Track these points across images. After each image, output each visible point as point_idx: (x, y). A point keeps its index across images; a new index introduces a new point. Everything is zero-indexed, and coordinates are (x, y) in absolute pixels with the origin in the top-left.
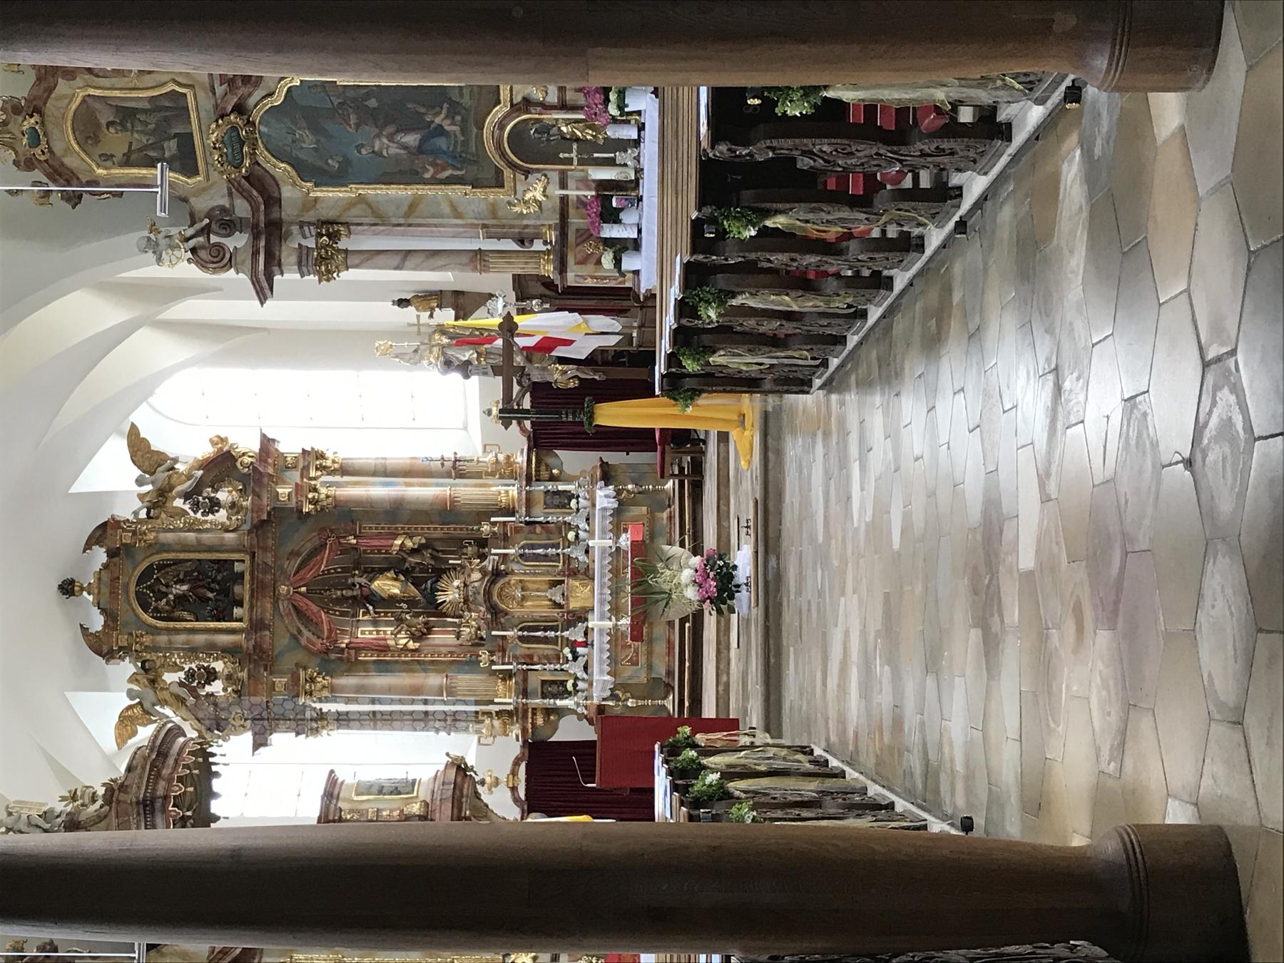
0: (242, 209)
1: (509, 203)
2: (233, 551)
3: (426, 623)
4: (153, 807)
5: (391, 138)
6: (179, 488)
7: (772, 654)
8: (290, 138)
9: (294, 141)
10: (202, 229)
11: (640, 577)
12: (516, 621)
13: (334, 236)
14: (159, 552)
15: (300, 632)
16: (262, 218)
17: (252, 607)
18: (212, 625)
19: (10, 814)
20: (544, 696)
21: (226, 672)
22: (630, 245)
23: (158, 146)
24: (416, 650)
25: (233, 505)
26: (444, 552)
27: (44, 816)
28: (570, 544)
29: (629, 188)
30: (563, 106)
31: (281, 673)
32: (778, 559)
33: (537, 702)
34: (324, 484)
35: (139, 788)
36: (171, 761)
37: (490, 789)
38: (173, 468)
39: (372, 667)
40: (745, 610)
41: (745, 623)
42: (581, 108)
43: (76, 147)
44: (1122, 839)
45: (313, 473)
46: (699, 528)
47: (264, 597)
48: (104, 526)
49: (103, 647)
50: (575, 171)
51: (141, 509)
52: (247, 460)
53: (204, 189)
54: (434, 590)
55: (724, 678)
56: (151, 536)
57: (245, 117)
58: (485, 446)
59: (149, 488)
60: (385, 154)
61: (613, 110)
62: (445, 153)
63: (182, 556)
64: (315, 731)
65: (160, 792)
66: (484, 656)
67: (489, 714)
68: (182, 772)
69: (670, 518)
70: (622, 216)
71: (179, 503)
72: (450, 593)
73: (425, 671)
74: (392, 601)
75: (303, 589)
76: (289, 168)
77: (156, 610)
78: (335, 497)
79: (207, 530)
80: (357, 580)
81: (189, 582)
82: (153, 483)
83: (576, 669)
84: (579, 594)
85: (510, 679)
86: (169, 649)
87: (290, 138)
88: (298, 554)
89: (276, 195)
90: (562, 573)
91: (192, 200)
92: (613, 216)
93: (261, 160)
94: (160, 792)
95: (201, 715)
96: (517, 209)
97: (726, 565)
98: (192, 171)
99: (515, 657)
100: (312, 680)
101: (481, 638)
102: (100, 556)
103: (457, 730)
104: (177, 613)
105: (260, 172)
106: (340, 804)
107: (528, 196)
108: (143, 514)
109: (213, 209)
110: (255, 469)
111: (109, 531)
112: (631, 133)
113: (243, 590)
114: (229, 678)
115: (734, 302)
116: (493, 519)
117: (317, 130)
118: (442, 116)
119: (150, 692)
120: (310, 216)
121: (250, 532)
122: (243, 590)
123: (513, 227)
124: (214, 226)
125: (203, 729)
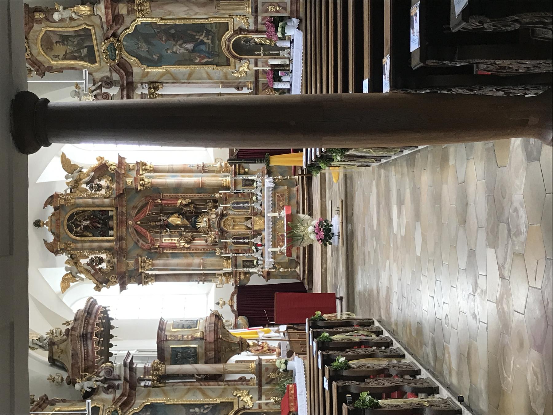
0: (116, 77)
1: (233, 73)
2: (108, 207)
3: (192, 236)
5: (181, 45)
7: (350, 266)
8: (136, 47)
9: (138, 48)
12: (231, 235)
13: (156, 88)
15: (138, 241)
16: (125, 82)
17: (117, 230)
18: (100, 238)
20: (244, 267)
21: (107, 259)
22: (286, 91)
23: (79, 51)
24: (188, 248)
25: (108, 187)
26: (199, 205)
27: (40, 339)
29: (286, 69)
30: (256, 31)
34: (147, 177)
35: (80, 329)
36: (93, 316)
38: (81, 171)
41: (336, 250)
42: (265, 32)
43: (42, 52)
45: (141, 172)
48: (52, 197)
50: (262, 59)
51: (68, 189)
52: (113, 167)
53: (99, 69)
54: (195, 222)
55: (325, 266)
56: (73, 201)
57: (117, 39)
59: (71, 179)
60: (178, 52)
61: (279, 35)
62: (204, 52)
63: (86, 209)
64: (146, 283)
65: (89, 330)
66: (218, 251)
67: (220, 275)
68: (98, 321)
69: (298, 190)
70: (282, 78)
71: (84, 186)
72: (202, 223)
73: (193, 256)
74: (177, 226)
75: (139, 222)
76: (136, 59)
77: (76, 232)
78: (151, 183)
79: (97, 198)
80: (162, 218)
82: (72, 178)
83: (257, 255)
84: (258, 224)
85: (229, 260)
86: (82, 249)
87: (136, 47)
91: (94, 74)
92: (278, 79)
93: (123, 56)
94: (89, 330)
95: (97, 277)
96: (236, 75)
98: (93, 61)
99: (231, 250)
100: (145, 262)
101: (216, 242)
102: (51, 209)
103: (207, 281)
104: (85, 233)
105: (124, 61)
106: (166, 333)
108: (69, 191)
109: (102, 78)
110: (116, 171)
111: (55, 199)
112: (287, 44)
113: (113, 223)
114: (109, 262)
115: (348, 153)
116: (220, 192)
117: (148, 42)
118: (203, 36)
119: (75, 268)
120: (146, 80)
121: (115, 198)
122: (113, 223)
125: (98, 283)
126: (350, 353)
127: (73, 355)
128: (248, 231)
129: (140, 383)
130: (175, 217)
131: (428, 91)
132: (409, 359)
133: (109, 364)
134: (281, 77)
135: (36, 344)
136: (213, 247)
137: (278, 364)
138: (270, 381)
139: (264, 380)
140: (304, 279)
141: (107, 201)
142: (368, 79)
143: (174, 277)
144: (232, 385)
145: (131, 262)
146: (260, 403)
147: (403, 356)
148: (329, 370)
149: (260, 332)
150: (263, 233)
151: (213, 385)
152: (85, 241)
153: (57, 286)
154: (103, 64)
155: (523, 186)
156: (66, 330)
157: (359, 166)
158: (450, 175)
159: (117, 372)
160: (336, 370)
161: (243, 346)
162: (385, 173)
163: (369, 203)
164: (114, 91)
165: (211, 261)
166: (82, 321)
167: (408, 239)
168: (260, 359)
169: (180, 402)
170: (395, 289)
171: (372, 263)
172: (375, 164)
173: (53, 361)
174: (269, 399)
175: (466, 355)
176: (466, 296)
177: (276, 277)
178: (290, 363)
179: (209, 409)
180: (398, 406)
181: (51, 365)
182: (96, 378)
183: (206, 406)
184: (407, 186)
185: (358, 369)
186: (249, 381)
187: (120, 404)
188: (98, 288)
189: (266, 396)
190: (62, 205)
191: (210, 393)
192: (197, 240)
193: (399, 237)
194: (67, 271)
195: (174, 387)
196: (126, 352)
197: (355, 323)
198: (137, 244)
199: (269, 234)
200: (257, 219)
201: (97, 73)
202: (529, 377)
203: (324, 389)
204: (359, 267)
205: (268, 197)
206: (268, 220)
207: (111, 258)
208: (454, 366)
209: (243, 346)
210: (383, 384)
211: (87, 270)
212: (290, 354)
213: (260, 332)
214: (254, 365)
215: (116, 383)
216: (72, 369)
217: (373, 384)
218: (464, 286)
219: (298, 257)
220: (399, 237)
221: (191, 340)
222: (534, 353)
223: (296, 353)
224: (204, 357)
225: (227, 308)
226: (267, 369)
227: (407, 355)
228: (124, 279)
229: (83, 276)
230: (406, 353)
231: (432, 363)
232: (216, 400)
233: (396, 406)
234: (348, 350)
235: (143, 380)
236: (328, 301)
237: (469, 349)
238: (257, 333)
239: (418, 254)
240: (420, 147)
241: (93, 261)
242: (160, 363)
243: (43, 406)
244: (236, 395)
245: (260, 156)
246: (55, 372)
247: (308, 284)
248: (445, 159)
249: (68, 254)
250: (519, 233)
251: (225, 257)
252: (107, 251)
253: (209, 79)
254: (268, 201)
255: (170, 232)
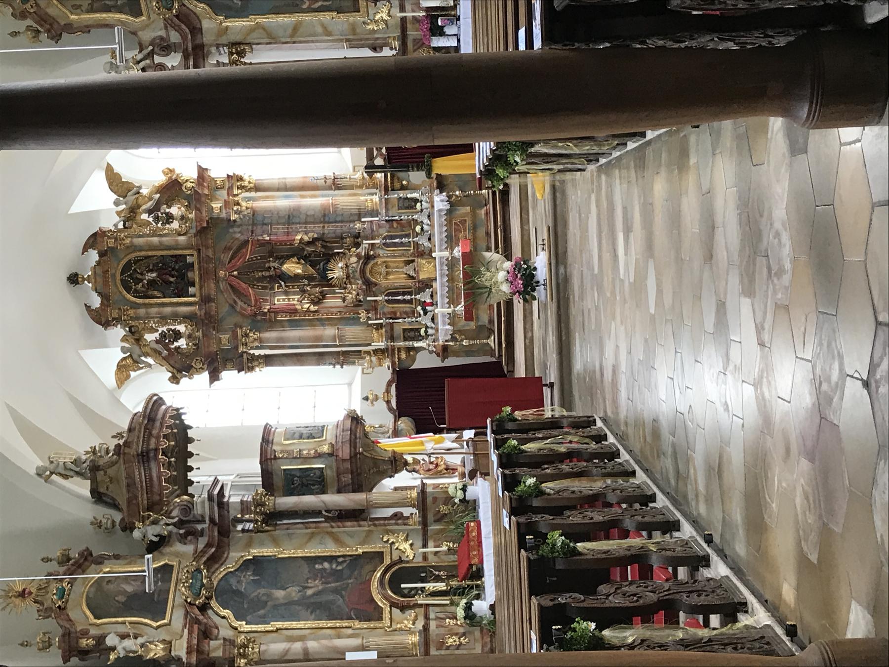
0: (175, 37)
1: (364, 23)
2: (185, 249)
3: (321, 292)
4: (148, 457)
6: (144, 207)
7: (563, 333)
10: (148, 54)
11: (469, 277)
13: (241, 54)
14: (134, 251)
15: (235, 302)
16: (190, 45)
17: (201, 288)
19: (52, 462)
20: (405, 339)
21: (187, 332)
25: (183, 218)
27: (76, 462)
28: (417, 235)
31: (225, 332)
32: (565, 267)
33: (401, 344)
35: (138, 444)
36: (158, 424)
37: (372, 403)
38: (139, 193)
39: (287, 324)
40: (543, 298)
41: (543, 307)
44: (822, 654)
45: (235, 192)
46: (507, 217)
47: (209, 279)
48: (95, 235)
49: (101, 318)
51: (119, 222)
52: (189, 185)
54: (325, 270)
55: (529, 334)
56: (128, 241)
58: (354, 167)
59: (124, 206)
63: (150, 253)
64: (251, 369)
66: (363, 315)
67: (368, 353)
69: (487, 214)
70: (445, 29)
71: (145, 216)
72: (337, 271)
73: (323, 325)
74: (297, 278)
75: (235, 273)
76: (207, 8)
77: (136, 291)
78: (252, 208)
79: (165, 235)
80: (272, 264)
81: (156, 271)
82: (125, 204)
83: (426, 320)
85: (382, 329)
88: (230, 249)
89: (198, 26)
90: (413, 255)
91: (140, 33)
92: (439, 32)
95: (172, 362)
96: (370, 27)
97: (529, 267)
98: (137, 13)
99: (384, 313)
100: (247, 335)
101: (360, 301)
102: (93, 256)
104: (150, 293)
106: (274, 448)
107: (377, 17)
108: (121, 226)
109: (154, 39)
111: (99, 239)
113: (194, 275)
114: (190, 337)
115: (533, 150)
116: (363, 220)
120: (224, 40)
121: (195, 235)
122: (194, 275)
123: (367, 39)
124: (156, 49)
125: (175, 371)
126: (548, 471)
127: (128, 485)
128: (410, 282)
129: (236, 527)
130: (293, 263)
131: (608, 45)
132: (641, 477)
133: (185, 497)
134: (442, 27)
135: (71, 470)
136: (357, 309)
137: (451, 491)
138: (440, 518)
139: (430, 517)
140: (500, 356)
141: (182, 238)
142: (524, 29)
143: (295, 358)
144: (380, 525)
145: (225, 337)
146: (425, 553)
147: (633, 474)
148: (511, 499)
149: (429, 442)
150: (434, 284)
151: (350, 526)
152: (151, 305)
153: (109, 377)
154: (153, 16)
155: (786, 195)
156: (116, 446)
157: (560, 171)
158: (691, 178)
159: (198, 510)
160: (521, 499)
161: (397, 463)
162: (606, 181)
163: (587, 231)
164: (173, 61)
165: (352, 332)
166: (140, 432)
167: (639, 287)
168: (423, 484)
169: (300, 553)
170: (623, 367)
171: (593, 327)
172: (592, 167)
173: (98, 496)
174: (439, 547)
175: (717, 470)
176: (715, 375)
177: (457, 354)
178: (470, 489)
179: (345, 565)
180: (609, 551)
181: (96, 502)
182: (165, 520)
183: (340, 560)
184: (636, 202)
185: (556, 496)
186: (408, 518)
187: (204, 559)
188: (175, 379)
189: (434, 541)
190: (112, 248)
191: (347, 540)
192: (330, 298)
193: (627, 284)
194: (124, 353)
195: (290, 531)
196: (212, 479)
197: (565, 422)
198: (233, 307)
199: (442, 285)
200: (424, 262)
201: (145, 32)
202: (799, 500)
203: (505, 528)
204: (577, 334)
205: (440, 226)
206: (441, 264)
207: (193, 330)
208: (701, 488)
209: (397, 463)
210: (592, 518)
211: (155, 351)
212: (472, 475)
213: (427, 442)
214: (414, 494)
215: (199, 527)
216: (128, 506)
217: (574, 518)
218: (711, 360)
219: (491, 321)
220: (627, 284)
221: (314, 457)
222: (804, 464)
223: (481, 474)
224: (336, 484)
225: (381, 405)
226: (435, 499)
227: (640, 473)
228: (216, 364)
229: (150, 360)
230: (637, 468)
231: (673, 482)
232: (357, 550)
233: (605, 553)
234: (546, 466)
235: (241, 521)
236: (531, 391)
237: (721, 457)
238: (422, 443)
239: (652, 311)
240: (650, 135)
241: (165, 336)
242: (267, 494)
243: (83, 567)
244: (388, 540)
245: (420, 159)
246: (103, 513)
247: (507, 365)
248: (684, 153)
249: (125, 326)
250: (781, 272)
251: (374, 324)
252: (187, 321)
253: (327, 35)
254: (441, 233)
255: (286, 286)
